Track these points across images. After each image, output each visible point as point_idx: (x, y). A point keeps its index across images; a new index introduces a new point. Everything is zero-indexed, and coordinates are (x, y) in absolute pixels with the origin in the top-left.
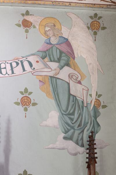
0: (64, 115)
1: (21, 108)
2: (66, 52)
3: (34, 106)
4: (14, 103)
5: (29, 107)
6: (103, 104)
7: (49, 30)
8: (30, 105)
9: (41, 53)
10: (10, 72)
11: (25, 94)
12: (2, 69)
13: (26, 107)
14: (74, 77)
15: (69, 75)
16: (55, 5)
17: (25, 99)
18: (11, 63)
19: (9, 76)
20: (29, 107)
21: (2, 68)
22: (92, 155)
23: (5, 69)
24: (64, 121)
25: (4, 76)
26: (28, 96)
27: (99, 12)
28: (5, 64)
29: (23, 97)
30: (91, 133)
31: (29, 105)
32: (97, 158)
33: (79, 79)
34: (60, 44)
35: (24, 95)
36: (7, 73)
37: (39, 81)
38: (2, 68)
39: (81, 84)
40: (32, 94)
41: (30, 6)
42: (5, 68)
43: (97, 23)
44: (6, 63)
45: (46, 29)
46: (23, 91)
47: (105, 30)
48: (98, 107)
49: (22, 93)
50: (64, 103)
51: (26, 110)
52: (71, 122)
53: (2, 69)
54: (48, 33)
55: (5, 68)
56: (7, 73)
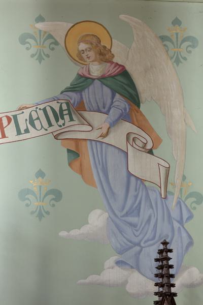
2: (114, 70)
7: (86, 50)
9: (185, 226)
10: (45, 124)
12: (35, 121)
14: (138, 142)
15: (128, 133)
18: (45, 108)
19: (47, 132)
21: (34, 119)
23: (38, 120)
24: (97, 103)
28: (36, 111)
30: (162, 245)
32: (175, 295)
33: (149, 147)
36: (42, 127)
37: (66, 150)
38: (34, 119)
39: (153, 155)
44: (38, 110)
45: (80, 46)
47: (161, 35)
50: (120, 191)
52: (134, 234)
53: (35, 121)
54: (84, 56)
55: (38, 118)
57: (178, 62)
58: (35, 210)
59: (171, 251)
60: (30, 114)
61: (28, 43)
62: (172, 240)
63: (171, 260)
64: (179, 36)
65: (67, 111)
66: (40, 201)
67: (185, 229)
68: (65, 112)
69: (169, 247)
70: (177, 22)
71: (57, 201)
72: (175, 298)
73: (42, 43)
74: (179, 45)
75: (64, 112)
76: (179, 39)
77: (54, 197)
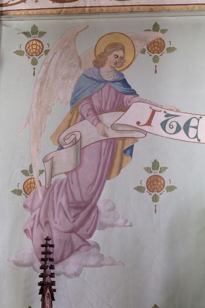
0: (39, 208)
1: (147, 196)
3: (170, 191)
4: (135, 188)
5: (161, 194)
6: (169, 185)
8: (163, 190)
11: (153, 171)
13: (157, 193)
16: (24, 15)
17: (154, 180)
20: (161, 194)
21: (190, 125)
22: (48, 279)
25: (191, 140)
26: (159, 174)
27: (41, 24)
29: (151, 176)
31: (161, 190)
34: (102, 82)
35: (29, 175)
36: (196, 137)
38: (190, 125)
40: (167, 170)
41: (50, 18)
42: (196, 128)
43: (38, 44)
46: (150, 166)
48: (160, 190)
49: (148, 170)
51: (155, 199)
53: (190, 128)
56: (196, 137)
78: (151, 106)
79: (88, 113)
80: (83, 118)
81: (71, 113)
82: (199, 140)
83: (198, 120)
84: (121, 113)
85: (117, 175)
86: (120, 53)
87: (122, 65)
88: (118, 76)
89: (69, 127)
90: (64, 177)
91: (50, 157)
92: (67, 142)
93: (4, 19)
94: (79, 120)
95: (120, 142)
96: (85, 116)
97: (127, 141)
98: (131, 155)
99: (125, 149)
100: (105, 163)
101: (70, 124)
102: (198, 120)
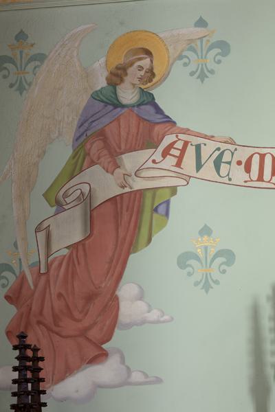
53: (222, 165)
55: (229, 163)
57: (21, 89)
58: (195, 70)
59: (42, 359)
60: (252, 156)
61: (190, 266)
62: (38, 340)
63: (42, 371)
64: (24, 55)
65: (179, 152)
66: (202, 58)
67: (73, 285)
68: (173, 152)
69: (40, 354)
70: (21, 36)
71: (224, 56)
72: (42, 408)
73: (208, 265)
74: (23, 67)
75: (178, 155)
76: (23, 60)
77: (220, 51)
78: (230, 182)
79: (182, 51)
80: (92, 163)
81: (74, 157)
82: (230, 179)
83: (233, 154)
84: (152, 150)
85: (147, 245)
86: (146, 63)
87: (150, 80)
88: (157, 128)
89: (72, 178)
90: (66, 252)
91: (45, 225)
92: (68, 200)
93: (136, 92)
94: (85, 164)
95: (149, 195)
96: (96, 161)
97: (159, 192)
98: (167, 214)
99: (155, 206)
100: (134, 201)
101: (74, 170)
102: (233, 154)
